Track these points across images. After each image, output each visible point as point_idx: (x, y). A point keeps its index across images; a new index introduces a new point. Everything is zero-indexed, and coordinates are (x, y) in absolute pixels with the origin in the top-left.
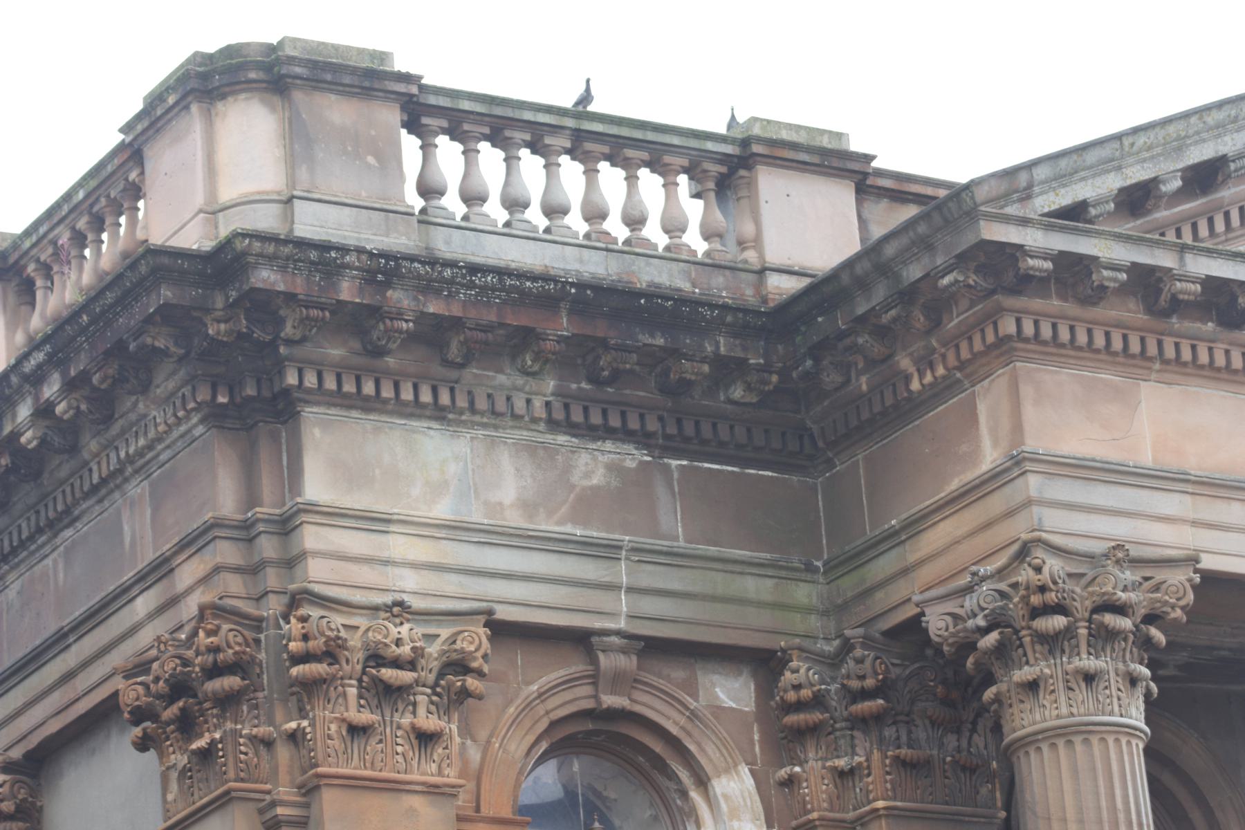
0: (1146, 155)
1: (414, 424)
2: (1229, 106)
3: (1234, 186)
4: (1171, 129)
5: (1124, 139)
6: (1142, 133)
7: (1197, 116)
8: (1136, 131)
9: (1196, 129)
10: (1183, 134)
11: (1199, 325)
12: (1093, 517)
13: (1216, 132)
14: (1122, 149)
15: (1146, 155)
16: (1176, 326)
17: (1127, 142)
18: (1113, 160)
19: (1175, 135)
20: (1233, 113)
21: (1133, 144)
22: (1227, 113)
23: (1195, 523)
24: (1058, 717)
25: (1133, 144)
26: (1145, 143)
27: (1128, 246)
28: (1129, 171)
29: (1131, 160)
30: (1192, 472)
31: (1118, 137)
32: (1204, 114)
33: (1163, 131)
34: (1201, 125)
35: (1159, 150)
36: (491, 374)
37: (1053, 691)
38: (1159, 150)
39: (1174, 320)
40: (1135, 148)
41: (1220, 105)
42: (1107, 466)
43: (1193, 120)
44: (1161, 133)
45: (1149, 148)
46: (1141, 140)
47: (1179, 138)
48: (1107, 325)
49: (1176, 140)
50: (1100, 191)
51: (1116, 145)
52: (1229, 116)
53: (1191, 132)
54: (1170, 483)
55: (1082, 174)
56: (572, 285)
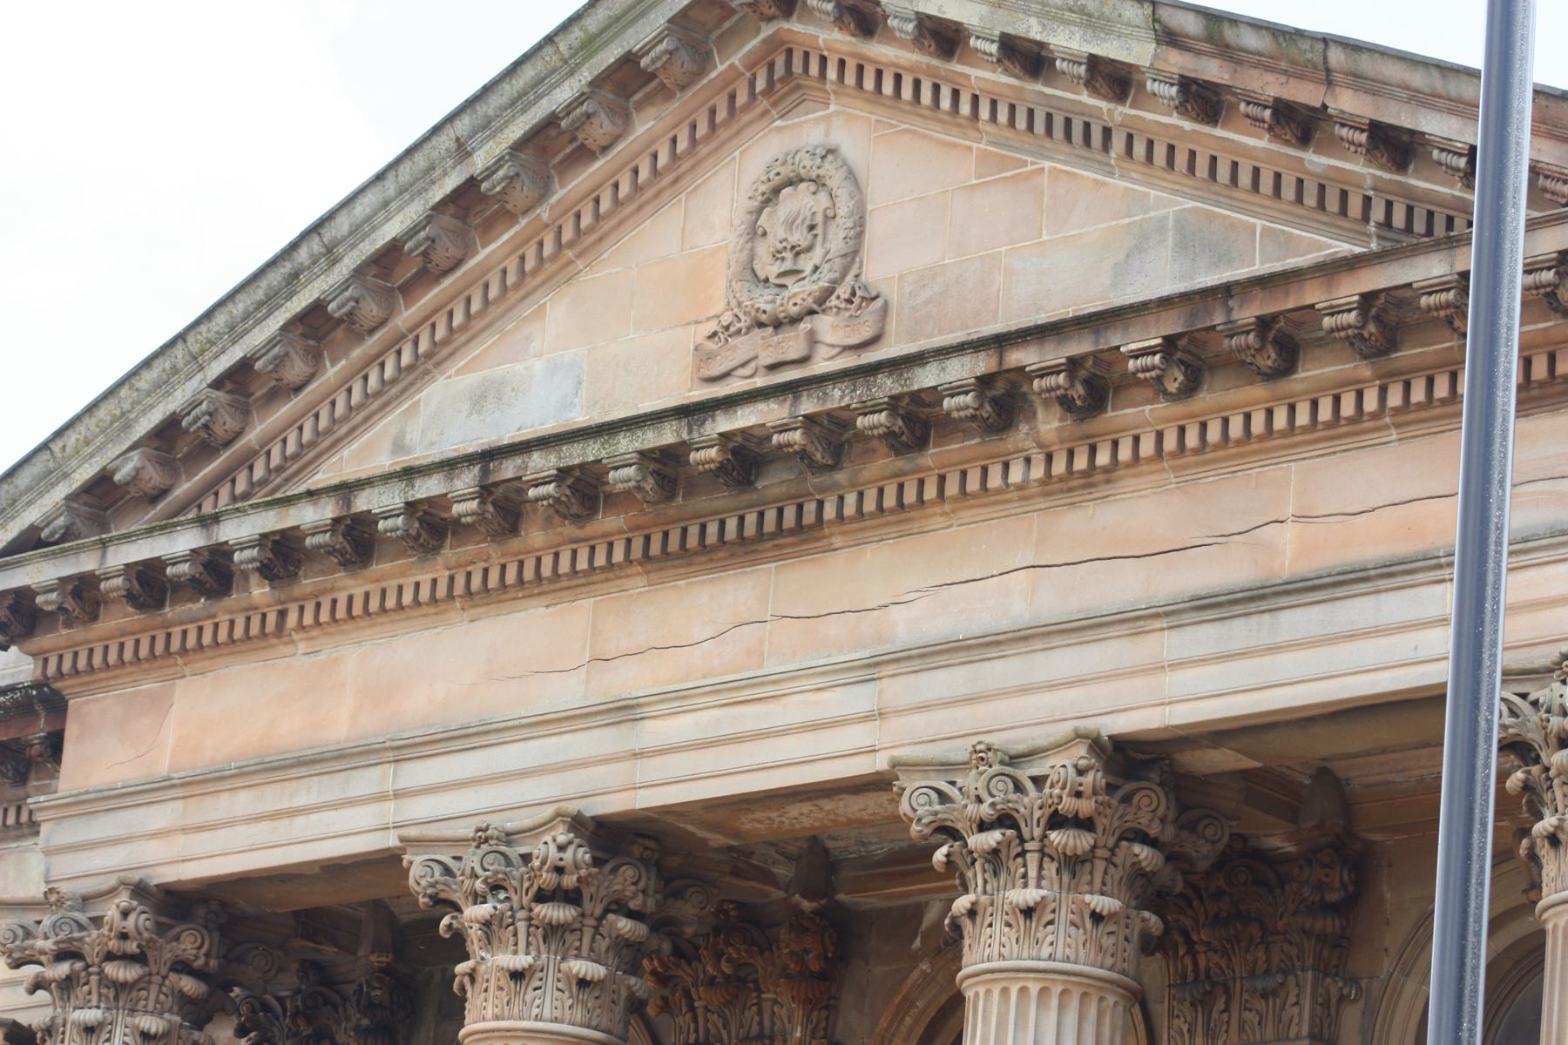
0: (89, 450)
1: (24, 843)
2: (161, 360)
3: (262, 421)
4: (102, 413)
5: (52, 446)
6: (70, 432)
7: (127, 386)
8: (59, 434)
9: (130, 400)
10: (118, 412)
11: (190, 605)
12: (96, 852)
13: (160, 392)
14: (53, 456)
15: (89, 450)
16: (169, 615)
17: (56, 447)
18: (50, 472)
19: (109, 418)
20: (167, 365)
21: (64, 448)
22: (160, 369)
23: (186, 830)
24: (1051, 957)
25: (64, 448)
26: (77, 440)
27: (57, 562)
28: (76, 476)
29: (74, 463)
30: (176, 775)
31: (45, 446)
32: (133, 381)
33: (93, 419)
34: (135, 394)
35: (101, 439)
36: (46, 782)
37: (1051, 922)
38: (101, 439)
39: (167, 609)
40: (68, 450)
41: (147, 363)
42: (99, 795)
43: (124, 392)
44: (90, 423)
45: (87, 443)
46: (72, 439)
47: (115, 419)
48: (133, 633)
49: (112, 423)
50: (46, 509)
51: (46, 455)
52: (164, 370)
53: (126, 406)
54: (156, 794)
55: (25, 499)
56: (32, 687)
